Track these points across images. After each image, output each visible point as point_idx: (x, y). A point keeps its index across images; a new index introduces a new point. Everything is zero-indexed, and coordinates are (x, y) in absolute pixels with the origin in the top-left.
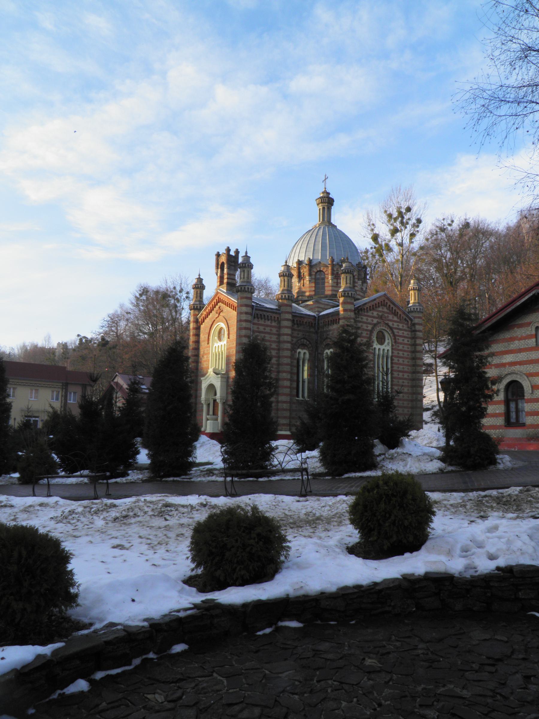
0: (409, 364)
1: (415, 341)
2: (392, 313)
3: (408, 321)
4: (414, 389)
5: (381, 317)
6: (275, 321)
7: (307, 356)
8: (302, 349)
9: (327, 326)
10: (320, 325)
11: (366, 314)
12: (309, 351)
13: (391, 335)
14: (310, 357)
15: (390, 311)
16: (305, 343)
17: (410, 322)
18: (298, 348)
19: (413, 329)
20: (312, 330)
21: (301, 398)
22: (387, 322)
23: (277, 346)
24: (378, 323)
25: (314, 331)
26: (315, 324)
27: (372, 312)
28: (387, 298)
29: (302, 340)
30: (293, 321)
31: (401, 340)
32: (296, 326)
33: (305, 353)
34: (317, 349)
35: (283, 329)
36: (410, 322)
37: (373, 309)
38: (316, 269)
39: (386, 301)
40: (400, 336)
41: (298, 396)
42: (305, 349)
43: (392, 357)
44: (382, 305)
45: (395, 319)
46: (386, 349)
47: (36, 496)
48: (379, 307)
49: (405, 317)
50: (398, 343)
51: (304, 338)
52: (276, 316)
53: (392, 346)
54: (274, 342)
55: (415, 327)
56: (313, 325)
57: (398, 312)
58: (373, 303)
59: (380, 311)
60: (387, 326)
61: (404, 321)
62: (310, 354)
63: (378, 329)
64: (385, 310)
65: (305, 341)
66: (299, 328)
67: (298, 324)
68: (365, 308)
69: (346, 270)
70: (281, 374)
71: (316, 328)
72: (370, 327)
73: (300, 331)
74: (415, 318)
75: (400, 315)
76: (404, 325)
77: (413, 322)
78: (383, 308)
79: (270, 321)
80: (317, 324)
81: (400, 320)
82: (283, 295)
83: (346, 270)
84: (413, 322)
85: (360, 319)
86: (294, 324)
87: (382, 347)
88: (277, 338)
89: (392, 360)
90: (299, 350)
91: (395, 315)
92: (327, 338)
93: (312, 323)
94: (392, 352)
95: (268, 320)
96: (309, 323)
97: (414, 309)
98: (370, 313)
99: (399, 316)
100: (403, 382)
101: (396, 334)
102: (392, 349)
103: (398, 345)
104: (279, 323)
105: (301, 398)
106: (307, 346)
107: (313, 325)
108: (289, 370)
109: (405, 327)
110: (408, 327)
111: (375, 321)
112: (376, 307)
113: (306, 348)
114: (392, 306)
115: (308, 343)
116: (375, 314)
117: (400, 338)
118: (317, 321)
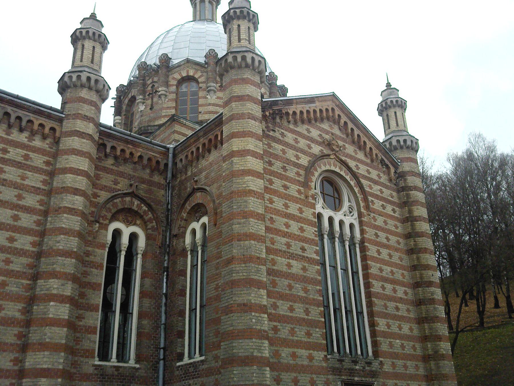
0: (404, 263)
1: (410, 211)
2: (353, 142)
3: (388, 167)
4: (426, 326)
5: (329, 145)
6: (44, 137)
7: (142, 243)
8: (128, 223)
9: (194, 164)
10: (179, 165)
11: (291, 126)
12: (145, 229)
13: (356, 190)
14: (147, 245)
15: (347, 136)
16: (135, 208)
17: (392, 170)
18: (114, 218)
19: (402, 184)
20: (157, 178)
21: (114, 361)
22: (343, 158)
23: (41, 202)
24: (324, 156)
25: (163, 182)
26: (166, 165)
27: (306, 126)
28: (337, 106)
29: (128, 199)
30: (101, 147)
31: (377, 205)
32: (110, 161)
33: (133, 237)
34: (169, 224)
35: (66, 157)
36: (392, 170)
37: (310, 121)
38: (180, 74)
39: (337, 112)
40: (377, 197)
41: (104, 355)
42: (135, 224)
43: (362, 242)
44: (328, 118)
45: (360, 155)
46: (348, 221)
47: (363, 311)
48: (322, 120)
49: (380, 156)
50: (374, 211)
51: (133, 195)
52: (49, 124)
53: (360, 215)
54: (36, 190)
55: (405, 180)
56: (162, 167)
57: (365, 142)
58: (306, 107)
59: (327, 132)
60: (344, 168)
61: (380, 166)
62: (148, 237)
63: (323, 166)
64: (336, 131)
65: (136, 202)
66: (121, 168)
67: (116, 158)
68: (291, 112)
69: (238, 11)
70: (40, 282)
71: (169, 175)
72: (304, 161)
73: (121, 174)
74: (403, 160)
75: (371, 149)
76: (382, 175)
77: (400, 170)
78: (330, 126)
79: (26, 134)
80: (170, 165)
81: (372, 161)
82: (72, 75)
83: (238, 11)
84: (400, 170)
85: (277, 135)
86: (106, 156)
87: (337, 217)
88: (44, 182)
89: (363, 249)
90: (116, 225)
91: (360, 148)
92: (194, 191)
93: (158, 162)
94: (362, 232)
95: (21, 130)
96: (150, 159)
97: (398, 141)
98: (302, 129)
99: (368, 149)
100: (397, 309)
101: (367, 189)
102: (361, 223)
103: (372, 215)
104: (57, 142)
105: (114, 361)
106: (141, 217)
107: (162, 167)
108: (70, 270)
109: (384, 179)
110: (390, 180)
111: (316, 149)
112: (316, 120)
113: (138, 222)
114: (350, 125)
115: (145, 208)
116: (315, 133)
117: (376, 201)
118: (171, 155)
